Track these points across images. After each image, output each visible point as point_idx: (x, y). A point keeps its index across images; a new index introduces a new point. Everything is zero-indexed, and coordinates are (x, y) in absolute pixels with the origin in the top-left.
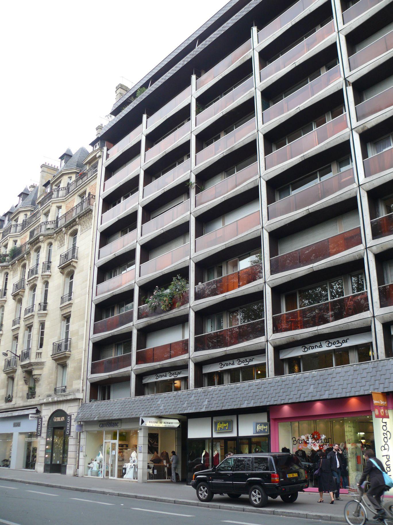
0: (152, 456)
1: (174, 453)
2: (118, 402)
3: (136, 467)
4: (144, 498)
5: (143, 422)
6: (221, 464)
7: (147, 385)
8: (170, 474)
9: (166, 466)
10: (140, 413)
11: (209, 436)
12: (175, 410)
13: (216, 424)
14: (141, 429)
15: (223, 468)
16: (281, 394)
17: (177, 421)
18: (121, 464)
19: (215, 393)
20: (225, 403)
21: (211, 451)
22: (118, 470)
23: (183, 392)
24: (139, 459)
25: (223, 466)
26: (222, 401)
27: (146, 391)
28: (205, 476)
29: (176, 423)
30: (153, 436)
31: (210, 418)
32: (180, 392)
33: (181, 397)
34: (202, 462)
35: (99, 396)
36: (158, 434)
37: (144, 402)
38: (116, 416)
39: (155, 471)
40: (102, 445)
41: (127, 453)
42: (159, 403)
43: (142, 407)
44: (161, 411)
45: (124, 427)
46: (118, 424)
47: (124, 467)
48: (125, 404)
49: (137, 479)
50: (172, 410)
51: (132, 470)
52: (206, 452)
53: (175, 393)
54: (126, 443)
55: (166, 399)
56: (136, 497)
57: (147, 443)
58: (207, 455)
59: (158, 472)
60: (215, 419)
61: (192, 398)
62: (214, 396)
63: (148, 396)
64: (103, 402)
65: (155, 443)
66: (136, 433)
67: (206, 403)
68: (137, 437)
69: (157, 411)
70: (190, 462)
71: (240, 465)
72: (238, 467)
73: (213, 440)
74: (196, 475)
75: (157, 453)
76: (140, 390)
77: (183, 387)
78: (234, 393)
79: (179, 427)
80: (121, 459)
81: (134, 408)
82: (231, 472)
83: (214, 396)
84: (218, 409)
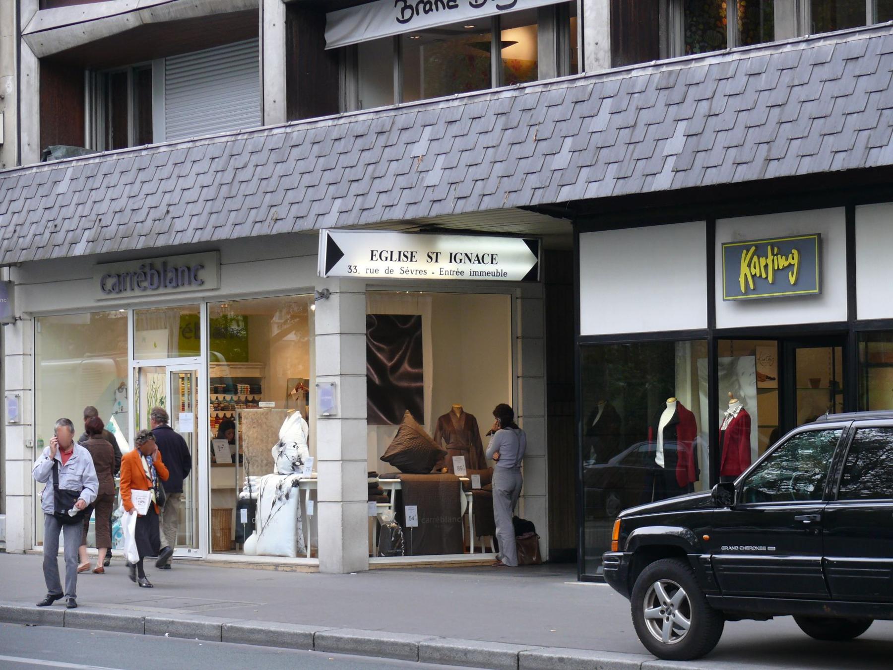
0: (388, 437)
1: (505, 415)
2: (195, 155)
3: (306, 493)
4: (358, 647)
5: (335, 254)
6: (762, 466)
7: (351, 56)
8: (486, 525)
9: (467, 486)
10: (317, 208)
11: (698, 321)
12: (507, 184)
13: (733, 254)
14: (325, 295)
15: (771, 484)
16: (791, 111)
17: (520, 247)
18: (226, 483)
19: (728, 87)
20: (781, 142)
21: (704, 401)
22: (215, 512)
23: (549, 91)
24: (321, 452)
25: (771, 473)
26: (765, 134)
27: (349, 88)
28: (679, 530)
29: (517, 258)
30: (393, 334)
31: (700, 228)
32: (531, 89)
33: (540, 114)
34: (660, 460)
35: (92, 124)
36: (419, 318)
37: (340, 147)
38: (187, 230)
39: (411, 514)
40: (123, 387)
41: (257, 423)
42: (419, 149)
43: (329, 177)
44: (430, 195)
45: (239, 286)
46: (202, 274)
47: (245, 494)
48: (234, 163)
49: (314, 555)
50: (491, 186)
51: (289, 509)
52: (679, 407)
53: (508, 93)
54: (247, 363)
55: (455, 129)
56: (314, 642)
57: (361, 365)
58: (684, 422)
59: (428, 514)
60: (727, 231)
61: (601, 121)
62: (719, 104)
63: (360, 118)
64: (116, 159)
65: (406, 367)
66: (302, 318)
67: (676, 144)
68: (307, 347)
69: (408, 196)
70: (591, 464)
71: (868, 468)
72: (855, 479)
73: (717, 344)
74: (629, 525)
75: (419, 417)
76: (315, 86)
77: (547, 63)
78: (833, 88)
79: (531, 276)
80: (224, 456)
81: (286, 183)
82: (817, 505)
83: (719, 104)
84: (743, 175)
